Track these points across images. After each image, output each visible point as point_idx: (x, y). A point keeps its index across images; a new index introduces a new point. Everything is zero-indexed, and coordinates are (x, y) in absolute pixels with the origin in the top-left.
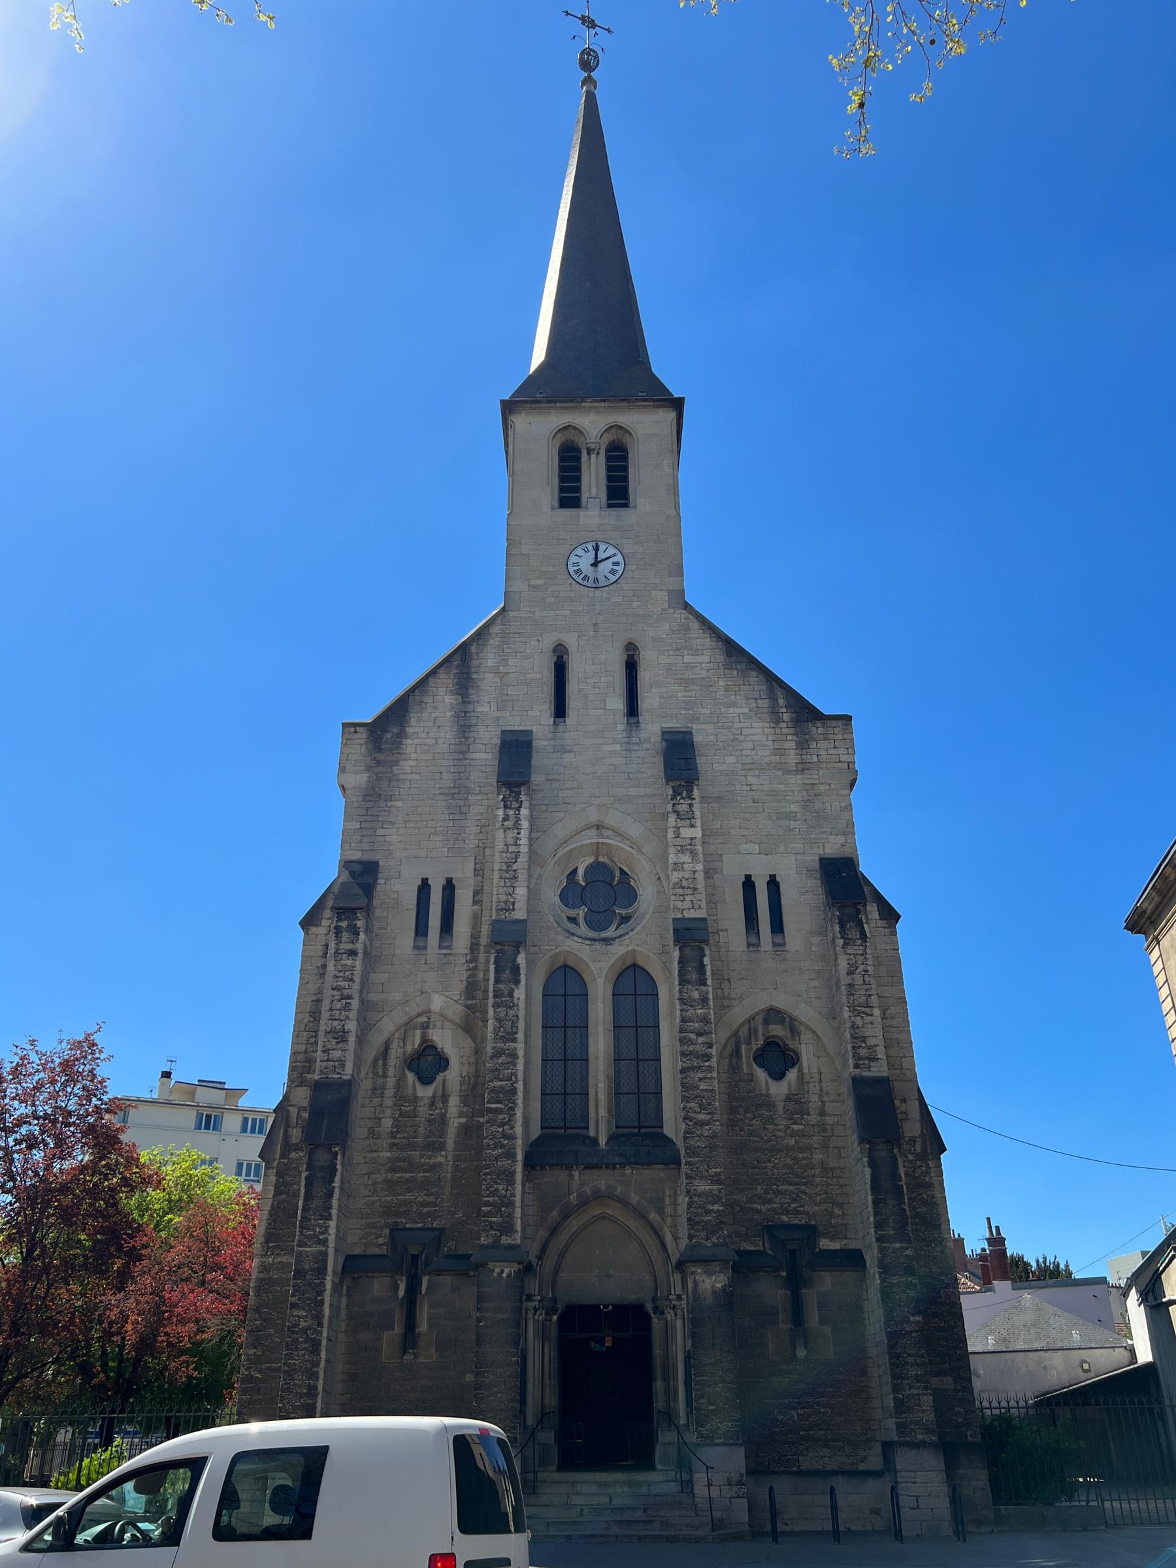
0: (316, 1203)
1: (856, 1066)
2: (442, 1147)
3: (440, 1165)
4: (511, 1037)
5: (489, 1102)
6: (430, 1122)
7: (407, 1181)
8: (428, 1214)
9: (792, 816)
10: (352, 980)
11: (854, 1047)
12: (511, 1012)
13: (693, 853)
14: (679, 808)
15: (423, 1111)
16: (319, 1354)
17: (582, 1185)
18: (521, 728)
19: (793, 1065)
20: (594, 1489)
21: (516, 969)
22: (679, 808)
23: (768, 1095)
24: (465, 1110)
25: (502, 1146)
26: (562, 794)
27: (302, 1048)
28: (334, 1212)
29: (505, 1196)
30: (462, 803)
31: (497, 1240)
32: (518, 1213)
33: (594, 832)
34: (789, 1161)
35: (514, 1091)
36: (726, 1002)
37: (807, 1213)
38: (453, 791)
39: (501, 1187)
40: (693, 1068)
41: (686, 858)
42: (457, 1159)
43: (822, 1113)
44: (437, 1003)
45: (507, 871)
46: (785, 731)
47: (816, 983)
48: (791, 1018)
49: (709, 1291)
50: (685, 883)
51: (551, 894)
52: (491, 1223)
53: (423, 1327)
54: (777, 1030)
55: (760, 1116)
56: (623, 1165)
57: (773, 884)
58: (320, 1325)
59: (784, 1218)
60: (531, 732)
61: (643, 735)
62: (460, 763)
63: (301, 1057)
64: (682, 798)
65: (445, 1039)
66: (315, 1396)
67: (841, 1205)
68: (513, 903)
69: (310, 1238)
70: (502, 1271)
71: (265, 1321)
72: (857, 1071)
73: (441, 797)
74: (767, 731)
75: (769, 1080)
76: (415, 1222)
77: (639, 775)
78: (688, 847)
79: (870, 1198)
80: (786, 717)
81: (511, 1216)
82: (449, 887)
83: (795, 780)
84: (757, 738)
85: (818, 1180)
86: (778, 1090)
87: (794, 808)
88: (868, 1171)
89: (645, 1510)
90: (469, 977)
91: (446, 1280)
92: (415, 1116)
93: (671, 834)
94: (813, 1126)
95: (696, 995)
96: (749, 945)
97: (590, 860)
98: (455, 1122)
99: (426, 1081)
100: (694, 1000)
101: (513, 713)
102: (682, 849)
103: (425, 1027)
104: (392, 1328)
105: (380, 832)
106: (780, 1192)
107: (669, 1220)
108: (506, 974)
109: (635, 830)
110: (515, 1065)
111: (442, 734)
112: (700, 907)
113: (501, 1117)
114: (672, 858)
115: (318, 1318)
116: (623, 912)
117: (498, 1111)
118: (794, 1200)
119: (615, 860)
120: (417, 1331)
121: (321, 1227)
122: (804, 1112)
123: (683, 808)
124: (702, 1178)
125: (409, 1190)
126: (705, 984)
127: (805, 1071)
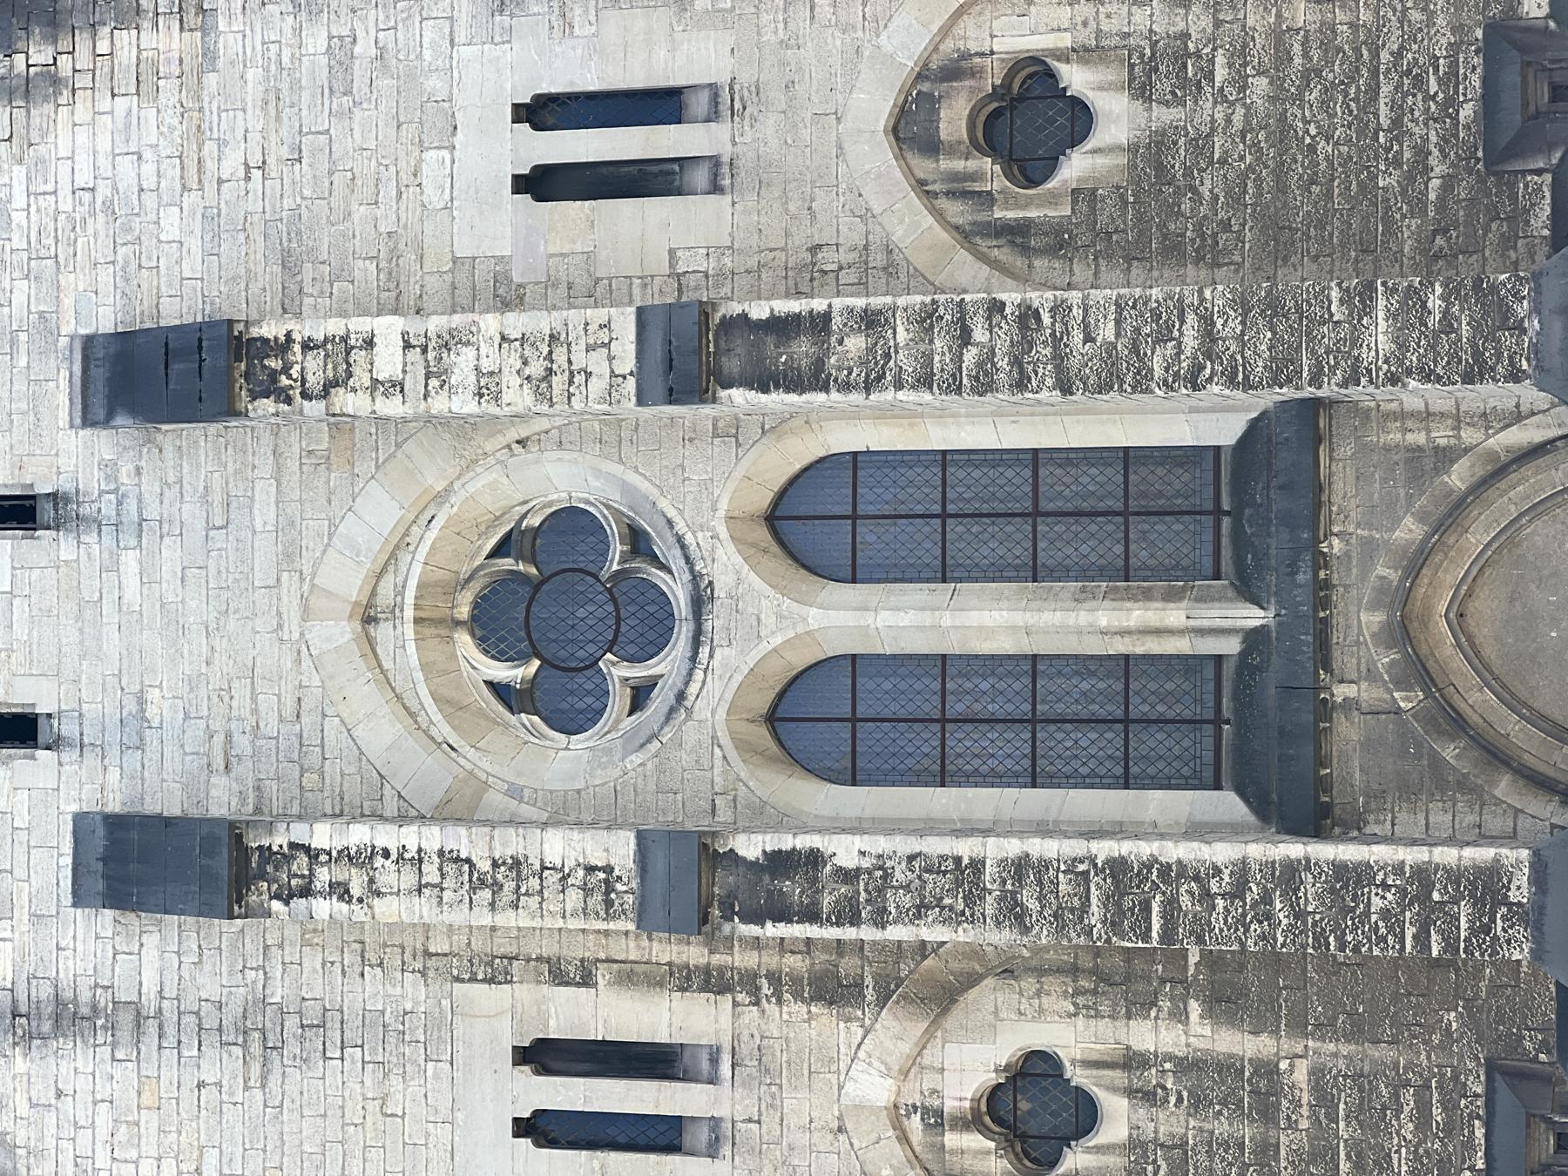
2: (1267, 1069)
3: (1317, 1074)
4: (968, 873)
5: (1146, 937)
6: (1198, 1103)
8: (1449, 1106)
9: (341, 52)
12: (900, 876)
13: (450, 342)
14: (314, 381)
15: (1170, 1122)
17: (1371, 675)
18: (67, 847)
19: (1051, 75)
21: (779, 862)
22: (314, 381)
23: (1133, 149)
24: (1166, 1004)
25: (1266, 898)
26: (270, 726)
29: (1402, 892)
30: (292, 1023)
31: (1517, 913)
32: (1446, 855)
33: (383, 632)
34: (1313, 96)
35: (1117, 866)
36: (878, 259)
38: (256, 1048)
39: (1377, 903)
40: (1059, 359)
41: (463, 363)
42: (1299, 1026)
44: (872, 1087)
45: (497, 887)
46: (84, 61)
48: (920, 77)
50: (536, 368)
51: (564, 760)
54: (954, 119)
55: (1188, 173)
56: (1321, 560)
57: (540, 112)
59: (1467, 112)
60: (79, 819)
61: (91, 481)
62: (170, 1030)
64: (286, 370)
65: (970, 1065)
68: (590, 869)
74: (82, 111)
75: (1090, 144)
76: (1469, 1145)
77: (217, 497)
78: (433, 356)
80: (41, 55)
81: (1454, 876)
82: (541, 1055)
84: (104, 144)
85: (1365, 16)
86: (1118, 119)
87: (316, 41)
90: (798, 996)
93: (391, 407)
94: (1218, 24)
96: (716, 188)
99: (1086, 1116)
100: (871, 350)
101: (20, 873)
102: (437, 374)
103: (936, 1120)
106: (1397, 123)
107: (1469, 436)
108: (793, 889)
109: (377, 512)
110: (1045, 864)
111: (84, 1084)
113: (1185, 901)
114: (465, 404)
116: (617, 549)
117: (1171, 905)
118: (1419, 82)
119: (465, 570)
122: (1179, 50)
123: (314, 369)
124: (1355, 342)
126: (827, 317)
127: (1066, 41)
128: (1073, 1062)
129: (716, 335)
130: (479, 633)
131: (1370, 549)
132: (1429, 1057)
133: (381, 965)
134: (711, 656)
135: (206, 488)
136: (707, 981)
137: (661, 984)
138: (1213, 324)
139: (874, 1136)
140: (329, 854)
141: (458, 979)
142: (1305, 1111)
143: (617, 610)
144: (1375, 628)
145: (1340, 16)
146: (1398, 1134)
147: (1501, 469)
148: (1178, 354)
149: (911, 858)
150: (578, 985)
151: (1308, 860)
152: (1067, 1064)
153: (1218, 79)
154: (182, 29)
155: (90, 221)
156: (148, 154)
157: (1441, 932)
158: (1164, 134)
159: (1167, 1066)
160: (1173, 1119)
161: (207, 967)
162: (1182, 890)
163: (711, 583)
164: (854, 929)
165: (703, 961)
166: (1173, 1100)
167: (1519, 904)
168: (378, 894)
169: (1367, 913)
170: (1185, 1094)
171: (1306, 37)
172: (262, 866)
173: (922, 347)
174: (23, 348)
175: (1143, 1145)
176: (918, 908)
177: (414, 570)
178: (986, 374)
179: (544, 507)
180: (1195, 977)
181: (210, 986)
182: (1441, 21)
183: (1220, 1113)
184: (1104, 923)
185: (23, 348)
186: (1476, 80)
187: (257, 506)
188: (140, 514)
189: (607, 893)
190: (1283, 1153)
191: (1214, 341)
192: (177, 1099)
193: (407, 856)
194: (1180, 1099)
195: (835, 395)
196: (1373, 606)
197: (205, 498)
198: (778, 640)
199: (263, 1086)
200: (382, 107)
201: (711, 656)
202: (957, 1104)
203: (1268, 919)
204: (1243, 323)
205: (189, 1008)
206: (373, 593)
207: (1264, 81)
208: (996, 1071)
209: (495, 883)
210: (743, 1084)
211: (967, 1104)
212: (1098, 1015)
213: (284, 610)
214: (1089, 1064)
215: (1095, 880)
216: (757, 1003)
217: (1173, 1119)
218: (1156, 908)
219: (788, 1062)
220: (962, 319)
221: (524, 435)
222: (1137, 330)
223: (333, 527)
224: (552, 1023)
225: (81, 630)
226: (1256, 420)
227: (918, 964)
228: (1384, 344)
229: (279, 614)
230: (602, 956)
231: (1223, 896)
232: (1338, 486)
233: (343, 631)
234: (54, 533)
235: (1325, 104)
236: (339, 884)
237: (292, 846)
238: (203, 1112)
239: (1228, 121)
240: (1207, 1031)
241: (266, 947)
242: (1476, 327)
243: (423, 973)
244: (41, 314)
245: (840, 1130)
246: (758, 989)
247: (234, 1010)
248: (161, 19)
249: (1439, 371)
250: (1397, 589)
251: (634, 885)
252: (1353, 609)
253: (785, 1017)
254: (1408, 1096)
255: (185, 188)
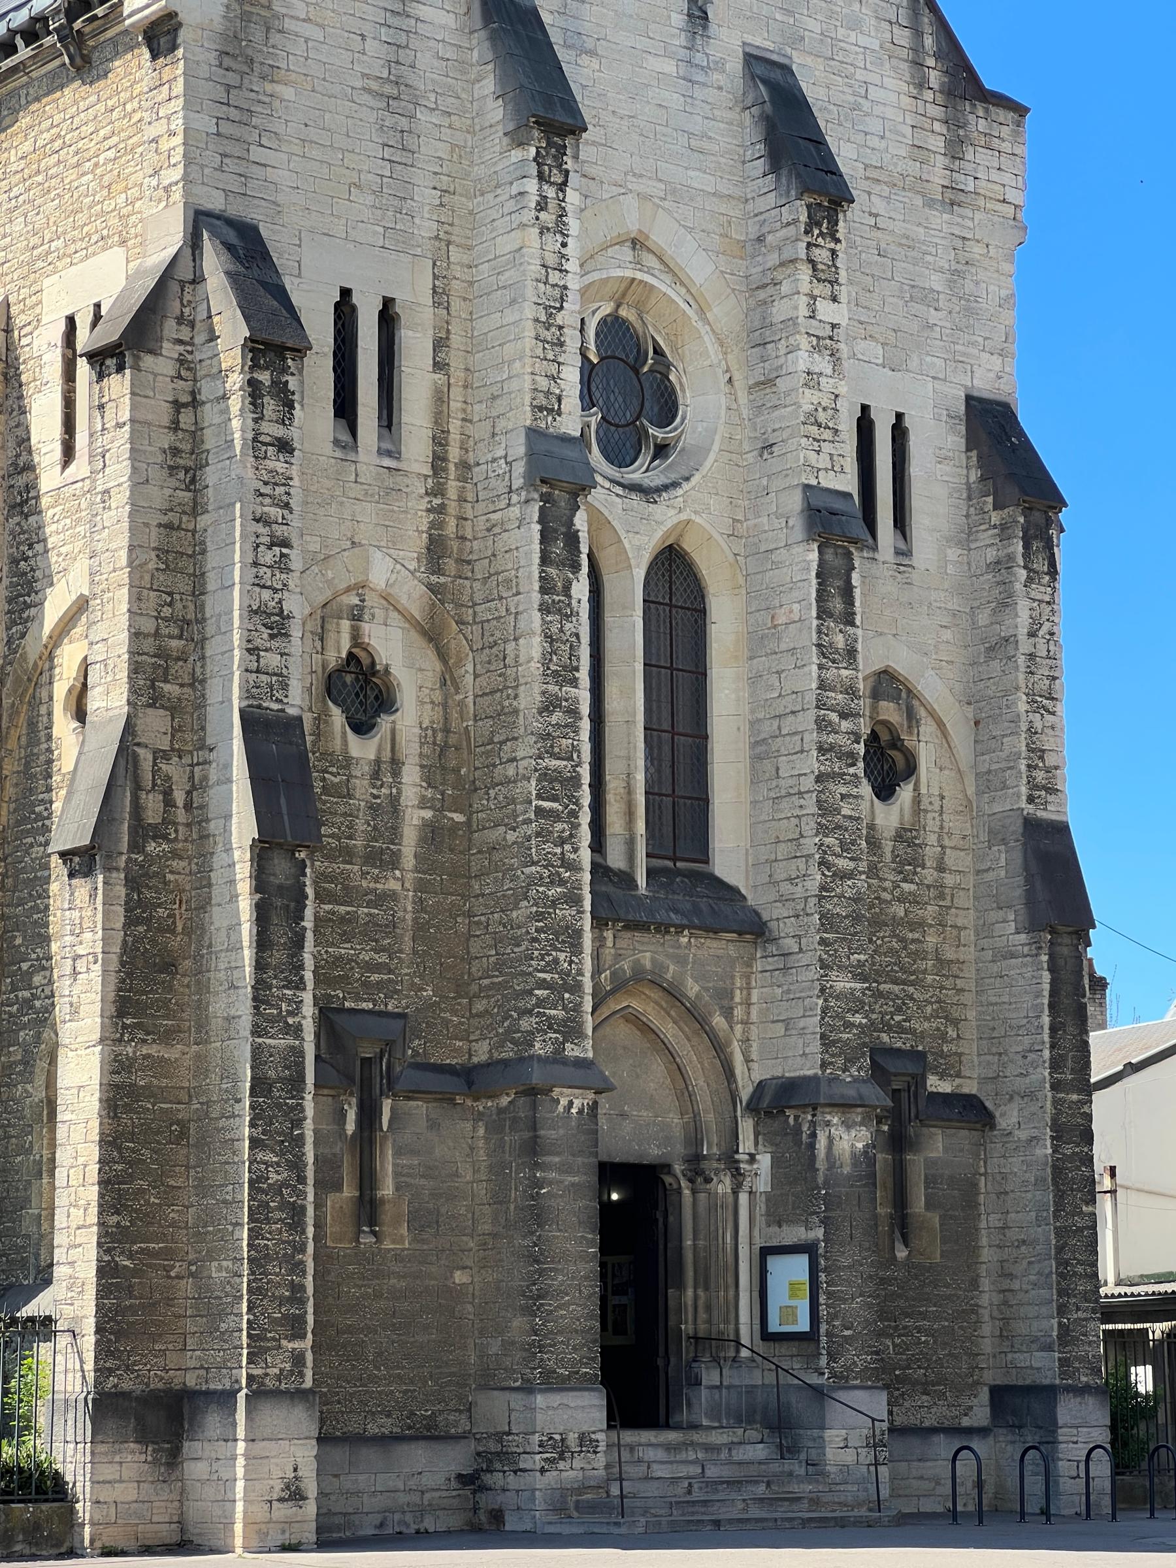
0: (277, 956)
1: (1031, 800)
2: (394, 862)
3: (393, 896)
7: (343, 920)
10: (287, 506)
11: (1029, 766)
15: (362, 787)
16: (303, 1232)
17: (618, 957)
20: (660, 1454)
24: (429, 793)
25: (562, 882)
27: (149, 626)
28: (308, 976)
29: (568, 974)
30: (404, 123)
31: (559, 1049)
33: (626, 253)
35: (575, 781)
37: (912, 1031)
39: (562, 956)
42: (421, 887)
43: (941, 868)
44: (380, 572)
47: (947, 635)
48: (909, 691)
49: (847, 1155)
50: (822, 417)
52: (549, 1017)
53: (387, 1189)
54: (890, 712)
56: (680, 928)
58: (302, 1180)
59: (885, 1037)
61: (715, 50)
63: (148, 645)
64: (821, 234)
65: (393, 647)
66: (302, 1302)
67: (955, 1022)
69: (272, 1020)
70: (571, 1103)
71: (130, 1164)
72: (1029, 809)
73: (367, 98)
74: (906, 101)
76: (358, 998)
77: (706, 145)
79: (1046, 1020)
83: (940, 219)
87: (936, 282)
88: (1046, 976)
89: (768, 1484)
90: (432, 525)
91: (419, 1108)
92: (350, 796)
94: (929, 887)
95: (840, 641)
97: (607, 309)
98: (414, 817)
99: (362, 727)
100: (837, 652)
103: (356, 615)
104: (338, 1187)
105: (256, 153)
107: (738, 1028)
108: (558, 548)
109: (700, 268)
112: (842, 471)
113: (559, 826)
115: (297, 1166)
117: (553, 815)
118: (899, 1010)
119: (648, 318)
120: (379, 1194)
121: (290, 1002)
122: (917, 862)
125: (346, 937)
127: (923, 791)
128: (394, 722)
129: (845, 547)
130: (609, 319)
131: (681, 961)
132: (406, 975)
133: (441, 205)
134: (617, 495)
135: (710, 138)
136: (439, 458)
137: (436, 423)
138: (849, 879)
139: (351, 569)
140: (563, 201)
141: (434, 264)
142: (372, 885)
143: (623, 426)
144: (642, 961)
145: (930, 963)
146: (362, 949)
147: (719, 1048)
148: (835, 854)
149: (577, 636)
150: (434, 359)
151: (583, 912)
152: (392, 718)
153: (904, 885)
154: (943, 186)
155: (850, 91)
156: (883, 144)
157: (548, 997)
158: (879, 848)
159: (394, 791)
160: (363, 791)
161: (436, 63)
162: (565, 825)
163: (656, 502)
164: (537, 588)
165: (451, 457)
166: (375, 791)
167: (564, 1049)
168: (541, 233)
169: (556, 949)
170: (379, 801)
171: (921, 942)
172: (555, 145)
173: (839, 686)
174: (785, 19)
175: (347, 767)
176: (551, 637)
177: (662, 284)
178: (826, 727)
179: (681, 383)
180: (445, 817)
181: (424, 60)
182: (926, 1025)
183: (369, 825)
184: (546, 768)
185: (785, 19)
186: (899, 1045)
187: (702, 175)
188: (697, 83)
189: (546, 409)
190: (348, 867)
191: (841, 879)
192: (353, 15)
193: (563, 261)
194: (376, 797)
195: (815, 622)
196: (653, 961)
197: (705, 136)
198: (626, 542)
199: (364, 89)
200: (904, 321)
201: (617, 495)
202: (367, 632)
203: (551, 882)
204: (850, 898)
205: (411, 40)
206: (649, 250)
207: (902, 914)
208: (387, 665)
209: (550, 325)
210: (378, 474)
211: (367, 640)
212: (422, 744)
213: (644, 180)
214: (393, 732)
215: (569, 764)
216: (427, 494)
217: (363, 791)
218: (555, 805)
219: (393, 511)
220: (852, 715)
221: (736, 384)
222: (846, 830)
223: (690, 230)
224: (410, 333)
225: (631, 16)
226: (739, 892)
227: (453, 618)
228: (839, 986)
229: (641, 176)
230: (452, 381)
231: (562, 853)
232: (715, 944)
233: (633, 226)
234: (686, 12)
235: (891, 950)
236: (546, 203)
237: (567, 172)
238: (346, 34)
239: (885, 890)
240: (415, 822)
241: (449, 114)
242: (846, 1043)
243: (437, 237)
244: (803, 38)
245: (353, 543)
246: (435, 496)
247: (412, 79)
248: (949, 173)
249: (827, 1019)
250: (661, 976)
251: (551, 430)
252: (652, 948)
253: (420, 513)
254: (383, 958)
255: (866, 167)
